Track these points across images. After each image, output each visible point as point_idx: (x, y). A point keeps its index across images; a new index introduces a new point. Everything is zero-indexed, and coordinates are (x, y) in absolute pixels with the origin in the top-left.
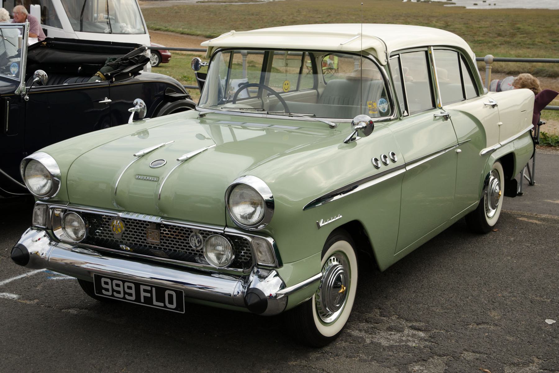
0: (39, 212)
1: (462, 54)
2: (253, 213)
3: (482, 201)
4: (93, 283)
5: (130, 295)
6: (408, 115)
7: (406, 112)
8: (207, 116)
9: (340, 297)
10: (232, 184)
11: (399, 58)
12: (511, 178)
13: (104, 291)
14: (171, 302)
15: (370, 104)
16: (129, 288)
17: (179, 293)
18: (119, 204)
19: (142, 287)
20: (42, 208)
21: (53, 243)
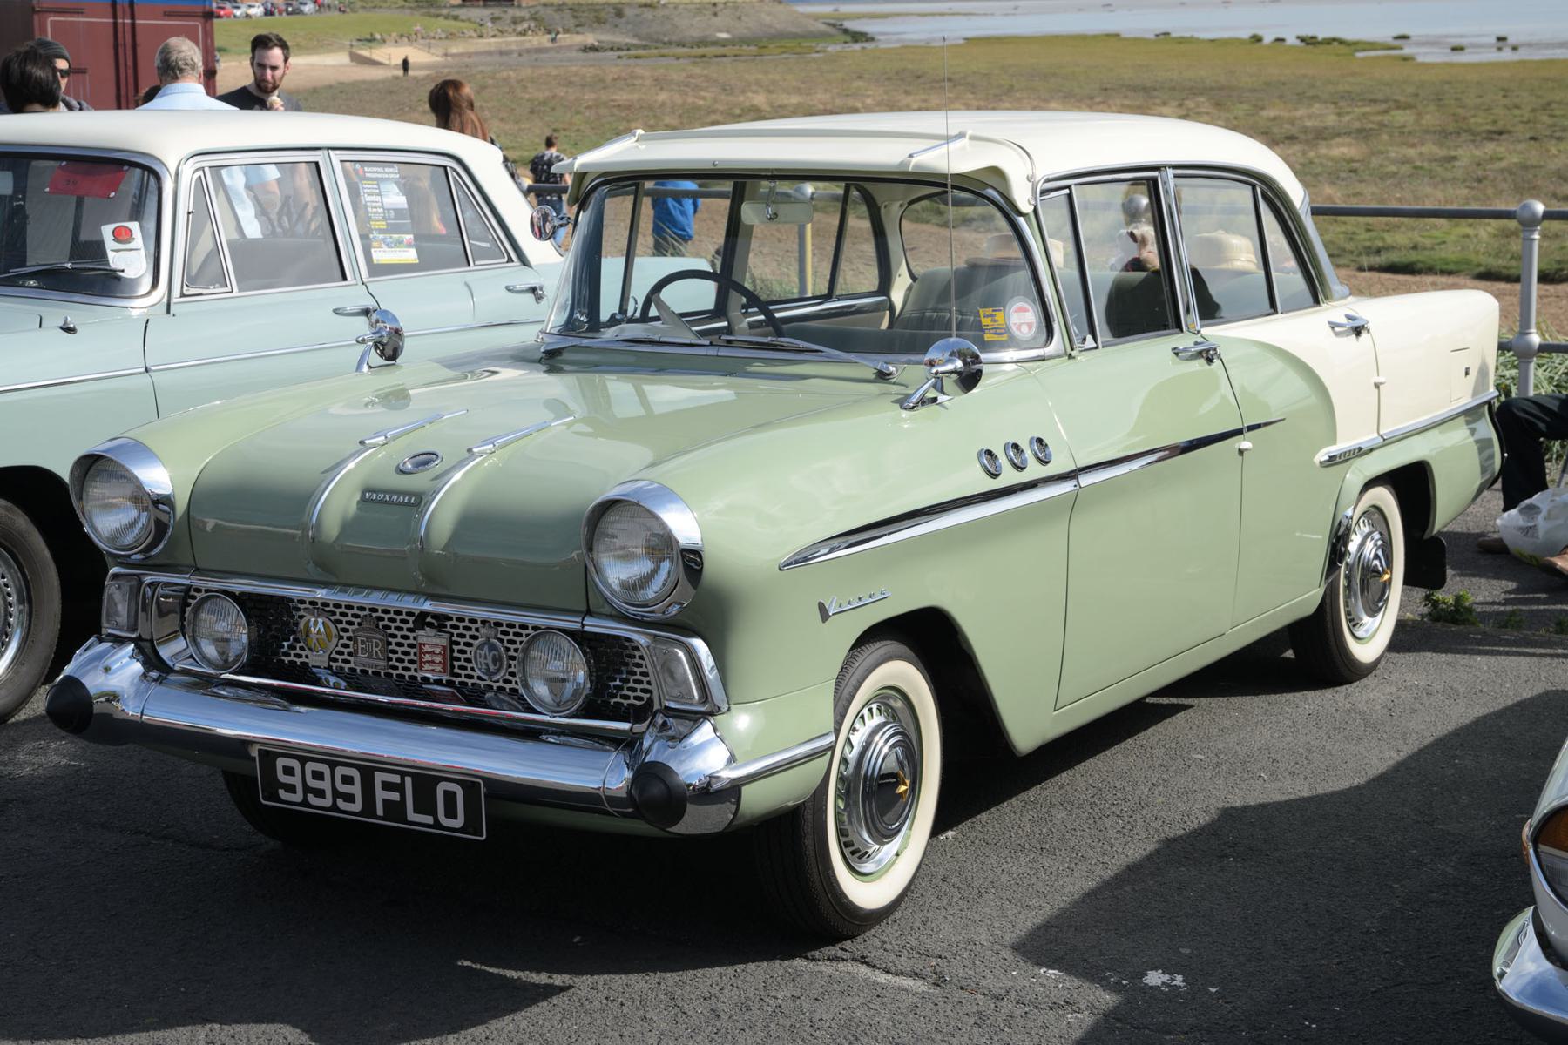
0: (117, 596)
1: (1268, 193)
2: (654, 572)
3: (1331, 594)
4: (257, 778)
5: (350, 798)
6: (1096, 348)
7: (1089, 338)
8: (565, 356)
9: (1050, 971)
10: (594, 503)
11: (1070, 196)
12: (1424, 532)
13: (282, 794)
14: (451, 813)
15: (988, 316)
16: (348, 780)
18: (321, 564)
19: (379, 777)
20: (126, 585)
21: (154, 674)
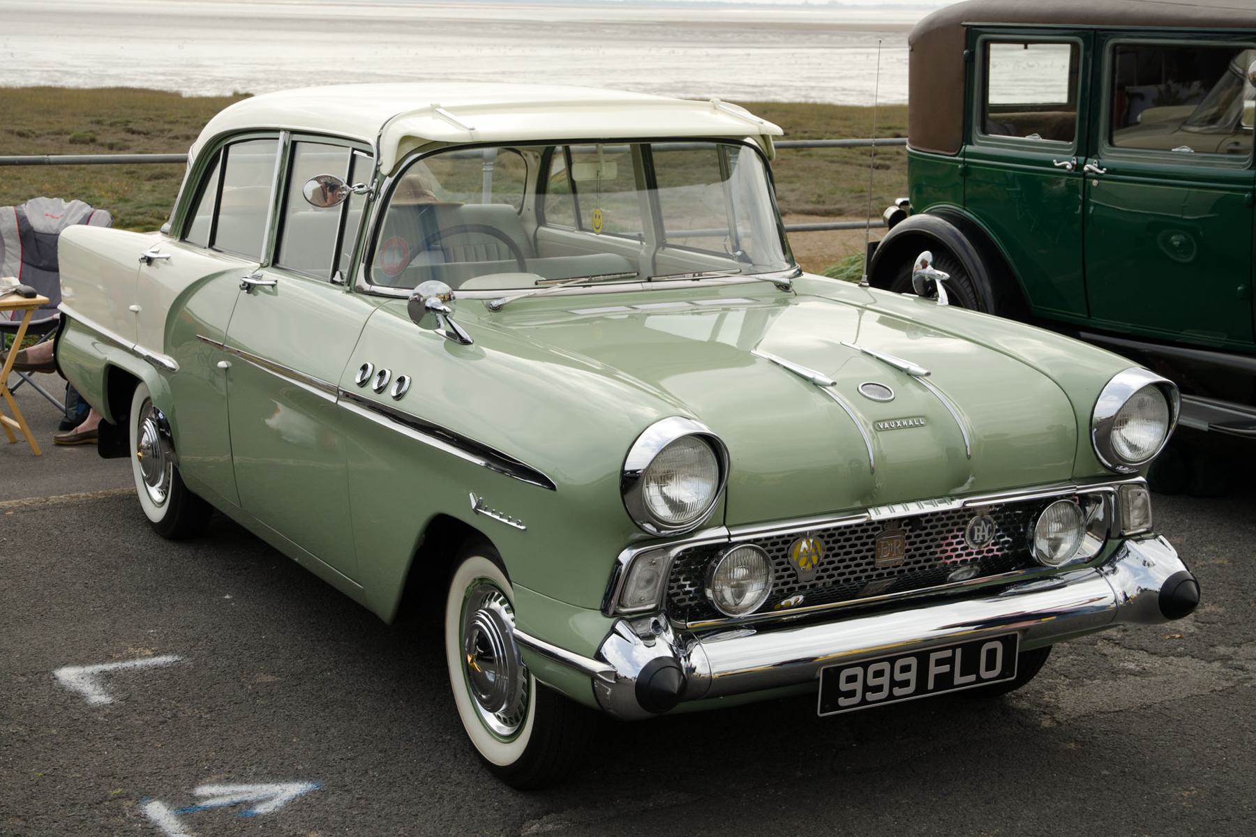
17: (1008, 641)
